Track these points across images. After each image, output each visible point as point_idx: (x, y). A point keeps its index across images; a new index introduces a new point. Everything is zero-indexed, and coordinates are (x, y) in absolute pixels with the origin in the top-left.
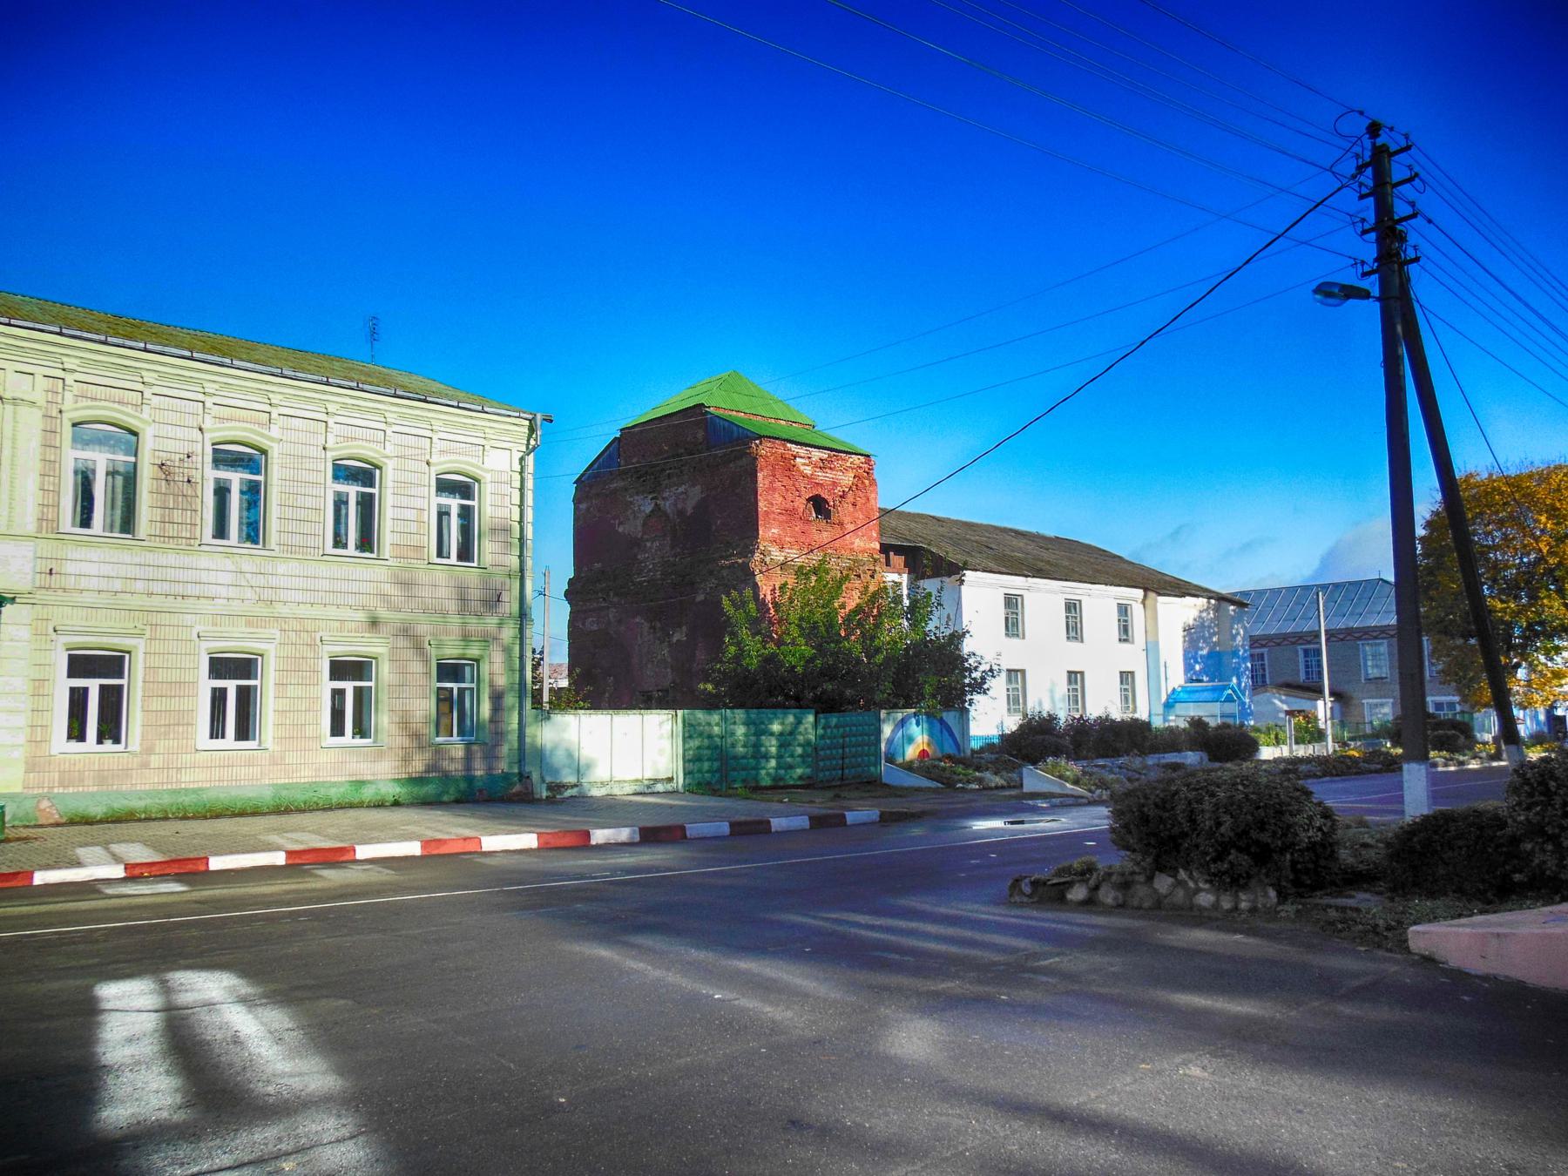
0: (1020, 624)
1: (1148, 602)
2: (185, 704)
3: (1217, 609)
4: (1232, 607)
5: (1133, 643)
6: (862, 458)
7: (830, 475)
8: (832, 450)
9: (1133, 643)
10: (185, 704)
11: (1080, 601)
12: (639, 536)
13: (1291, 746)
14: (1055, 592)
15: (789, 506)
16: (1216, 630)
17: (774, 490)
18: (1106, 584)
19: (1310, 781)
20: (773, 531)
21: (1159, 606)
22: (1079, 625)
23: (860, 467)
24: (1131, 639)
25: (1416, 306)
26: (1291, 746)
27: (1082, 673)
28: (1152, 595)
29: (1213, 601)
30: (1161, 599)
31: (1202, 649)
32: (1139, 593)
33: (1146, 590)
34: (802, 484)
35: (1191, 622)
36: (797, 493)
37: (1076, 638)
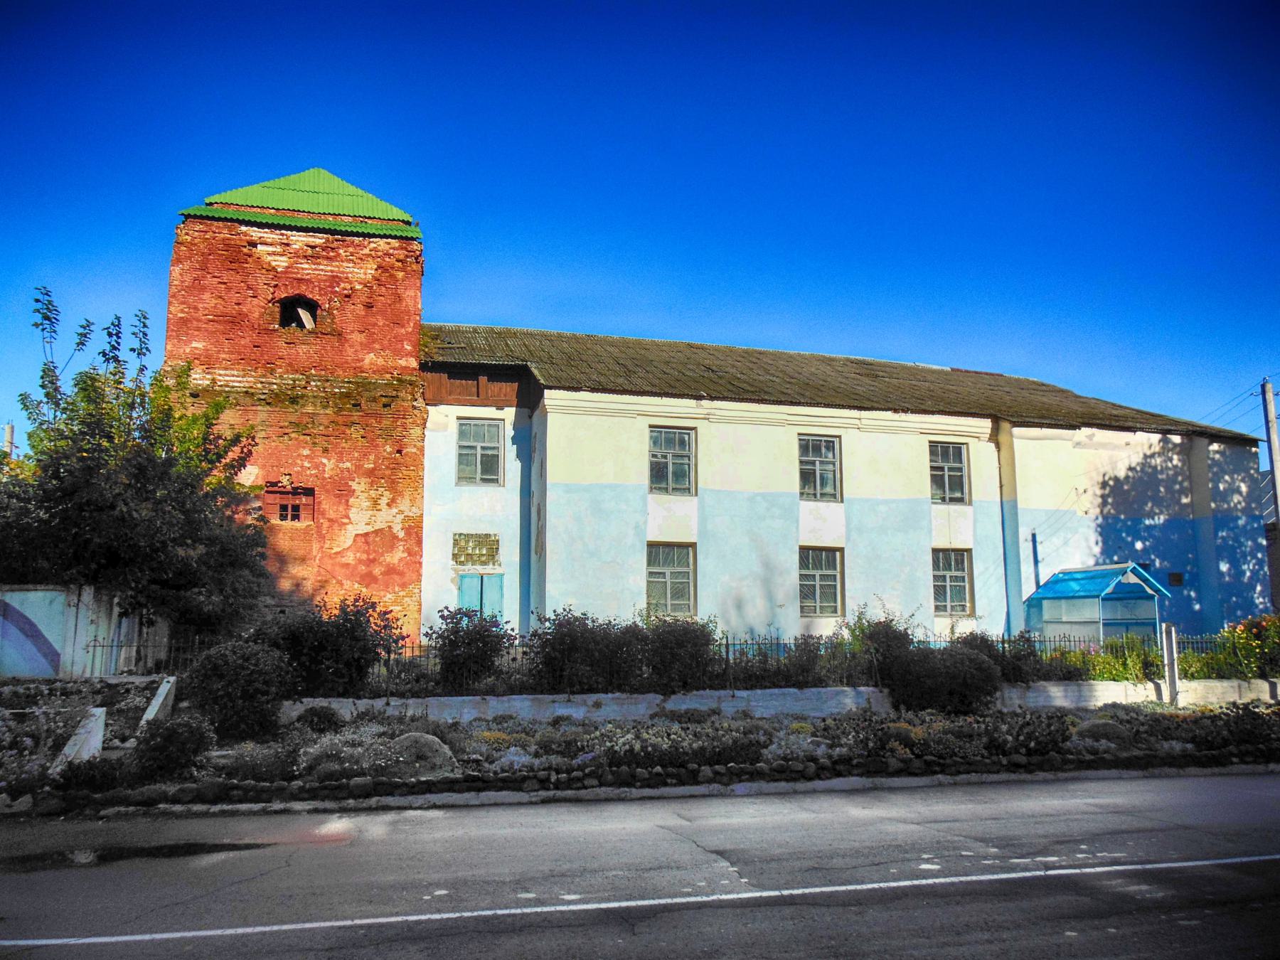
0: (693, 474)
1: (1003, 438)
2: (677, 447)
3: (1184, 450)
4: (1215, 447)
5: (970, 503)
6: (395, 243)
7: (326, 268)
8: (332, 232)
9: (970, 503)
10: (677, 447)
11: (839, 437)
12: (278, 305)
13: (1173, 684)
14: (781, 424)
15: (232, 309)
16: (1186, 484)
17: (203, 289)
18: (896, 411)
19: (67, 750)
20: (194, 344)
21: (1017, 443)
22: (838, 476)
23: (390, 255)
24: (966, 497)
25: (360, 192)
26: (1173, 684)
27: (841, 550)
28: (1005, 426)
29: (1176, 439)
30: (1017, 431)
31: (1151, 515)
32: (986, 425)
33: (996, 420)
34: (261, 280)
35: (1122, 474)
36: (250, 293)
37: (834, 496)
